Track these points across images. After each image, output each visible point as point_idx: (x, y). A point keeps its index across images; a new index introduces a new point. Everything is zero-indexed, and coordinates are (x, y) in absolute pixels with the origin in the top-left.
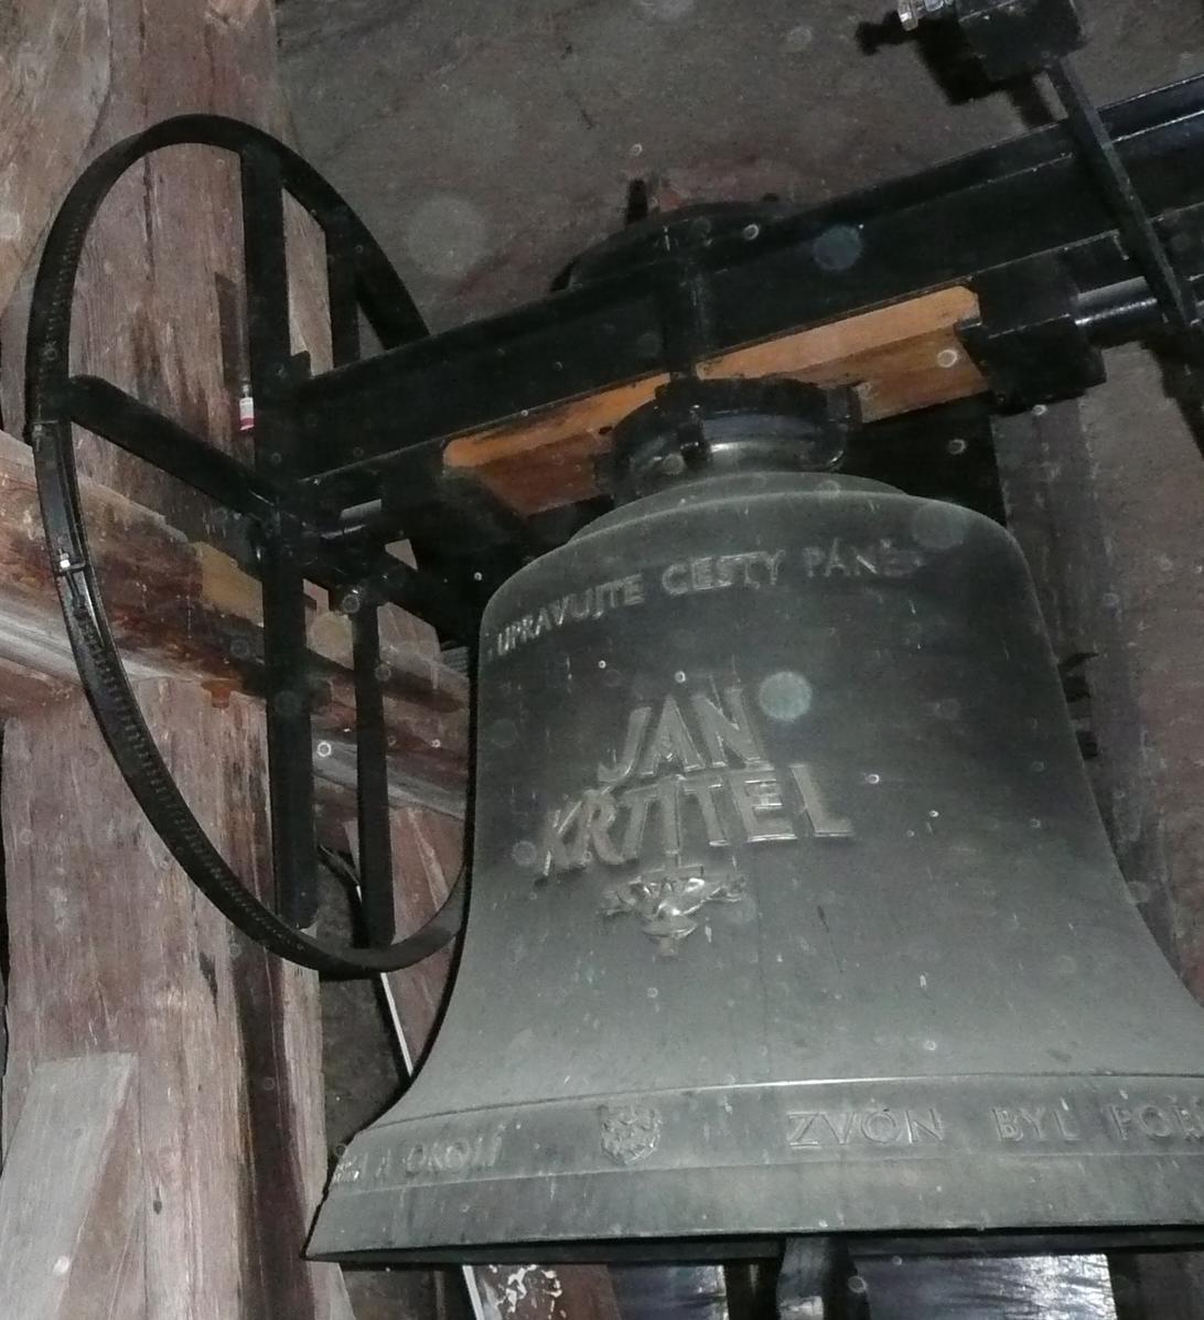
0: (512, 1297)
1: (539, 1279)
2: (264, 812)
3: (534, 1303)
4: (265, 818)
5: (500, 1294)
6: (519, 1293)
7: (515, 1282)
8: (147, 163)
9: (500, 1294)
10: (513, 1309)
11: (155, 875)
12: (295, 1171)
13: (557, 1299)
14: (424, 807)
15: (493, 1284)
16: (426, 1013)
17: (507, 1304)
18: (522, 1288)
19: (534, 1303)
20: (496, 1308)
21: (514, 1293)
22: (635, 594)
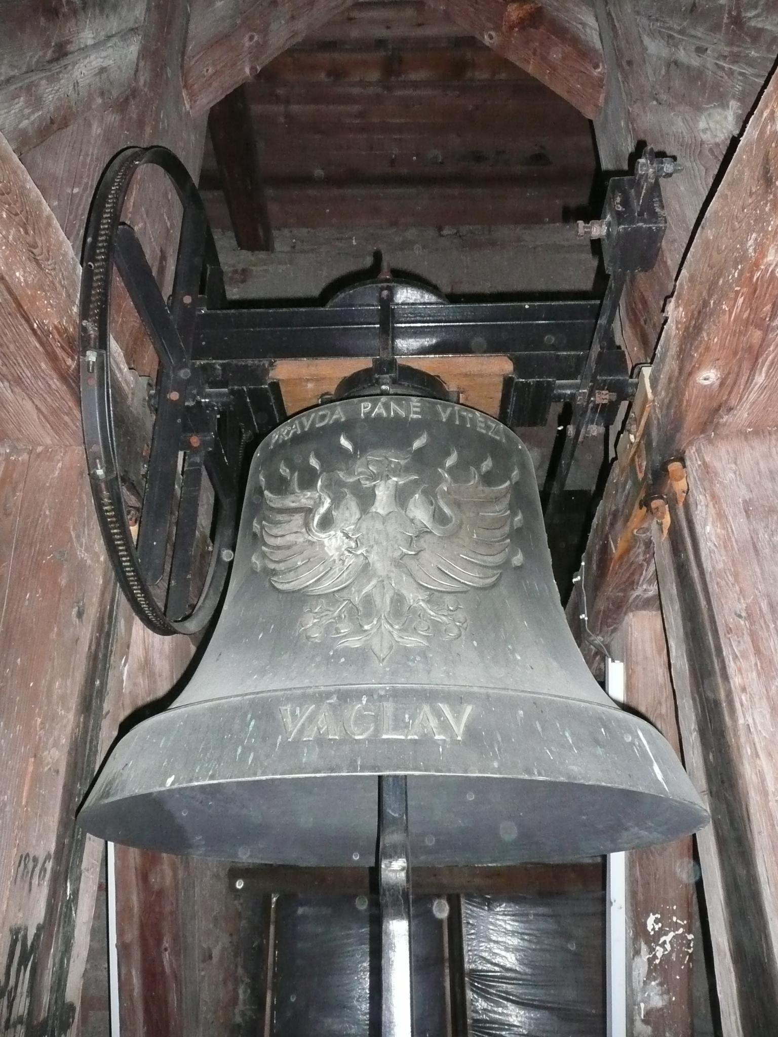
0: (659, 952)
1: (682, 940)
2: (444, 988)
3: (674, 958)
4: (444, 994)
5: (652, 950)
6: (665, 950)
7: (665, 942)
8: (716, 157)
9: (652, 950)
10: (657, 961)
11: (608, 771)
12: (734, 756)
13: (691, 955)
14: (587, 423)
15: (648, 943)
16: (697, 193)
17: (655, 957)
18: (668, 947)
19: (674, 958)
20: (646, 960)
21: (662, 950)
22: (417, 407)
